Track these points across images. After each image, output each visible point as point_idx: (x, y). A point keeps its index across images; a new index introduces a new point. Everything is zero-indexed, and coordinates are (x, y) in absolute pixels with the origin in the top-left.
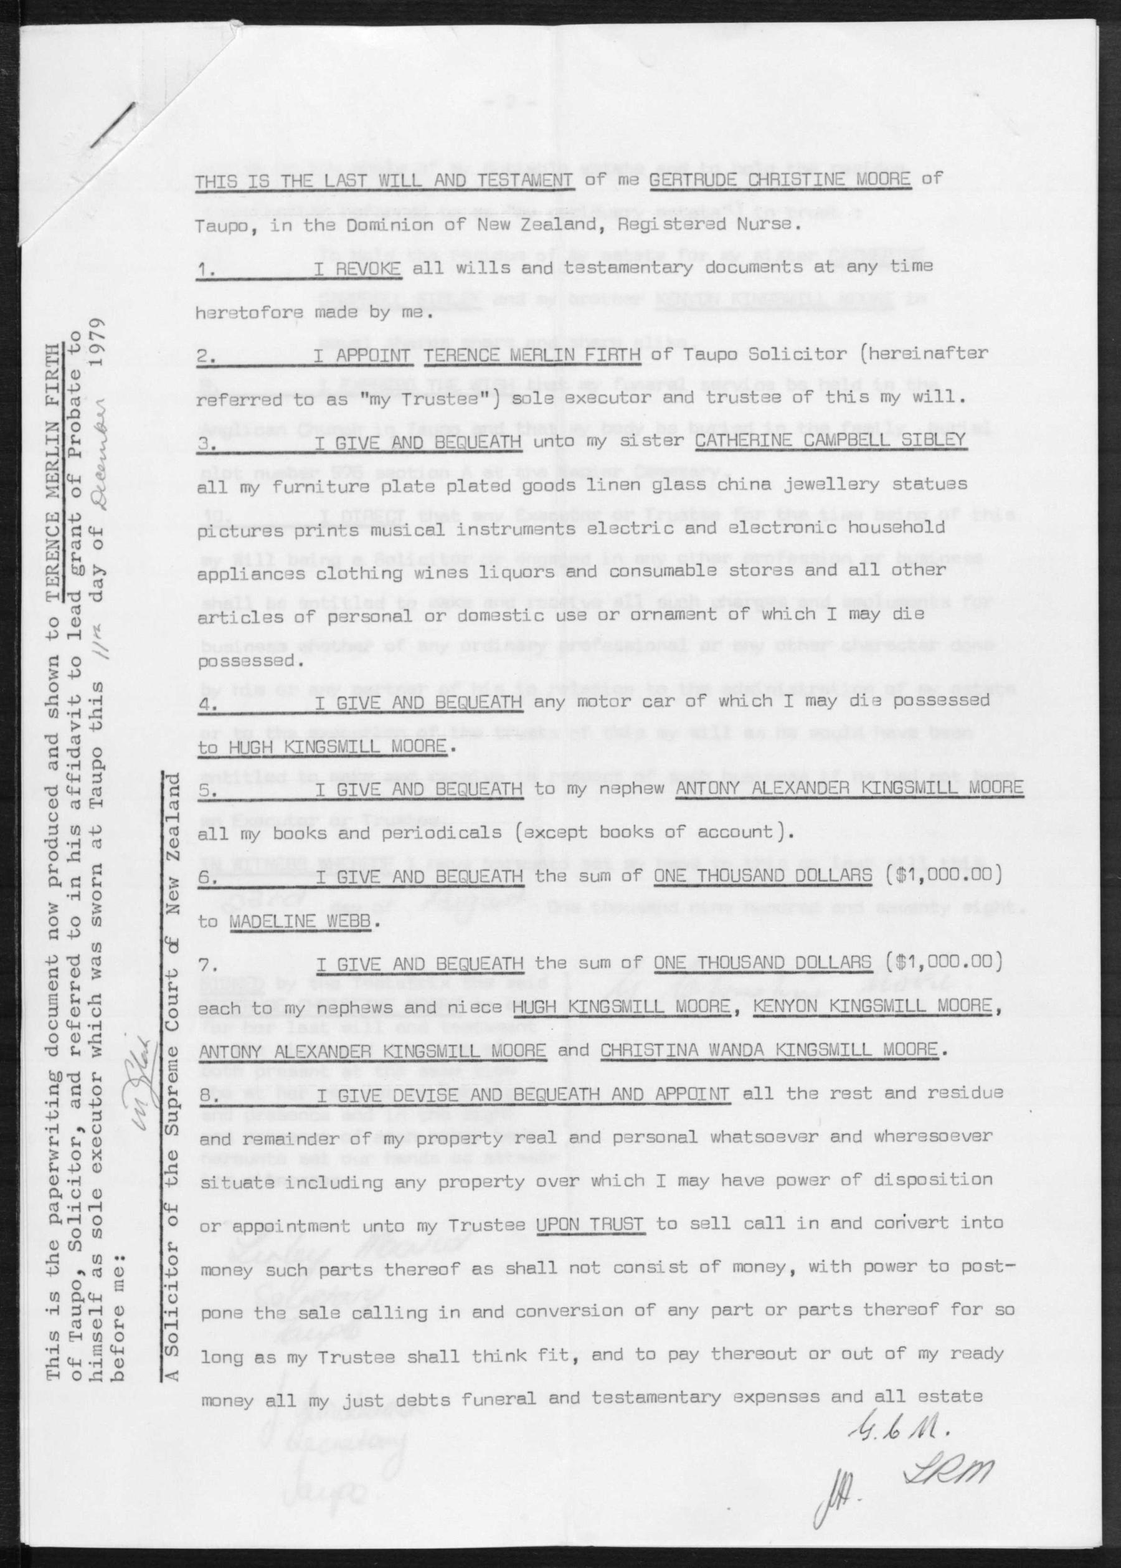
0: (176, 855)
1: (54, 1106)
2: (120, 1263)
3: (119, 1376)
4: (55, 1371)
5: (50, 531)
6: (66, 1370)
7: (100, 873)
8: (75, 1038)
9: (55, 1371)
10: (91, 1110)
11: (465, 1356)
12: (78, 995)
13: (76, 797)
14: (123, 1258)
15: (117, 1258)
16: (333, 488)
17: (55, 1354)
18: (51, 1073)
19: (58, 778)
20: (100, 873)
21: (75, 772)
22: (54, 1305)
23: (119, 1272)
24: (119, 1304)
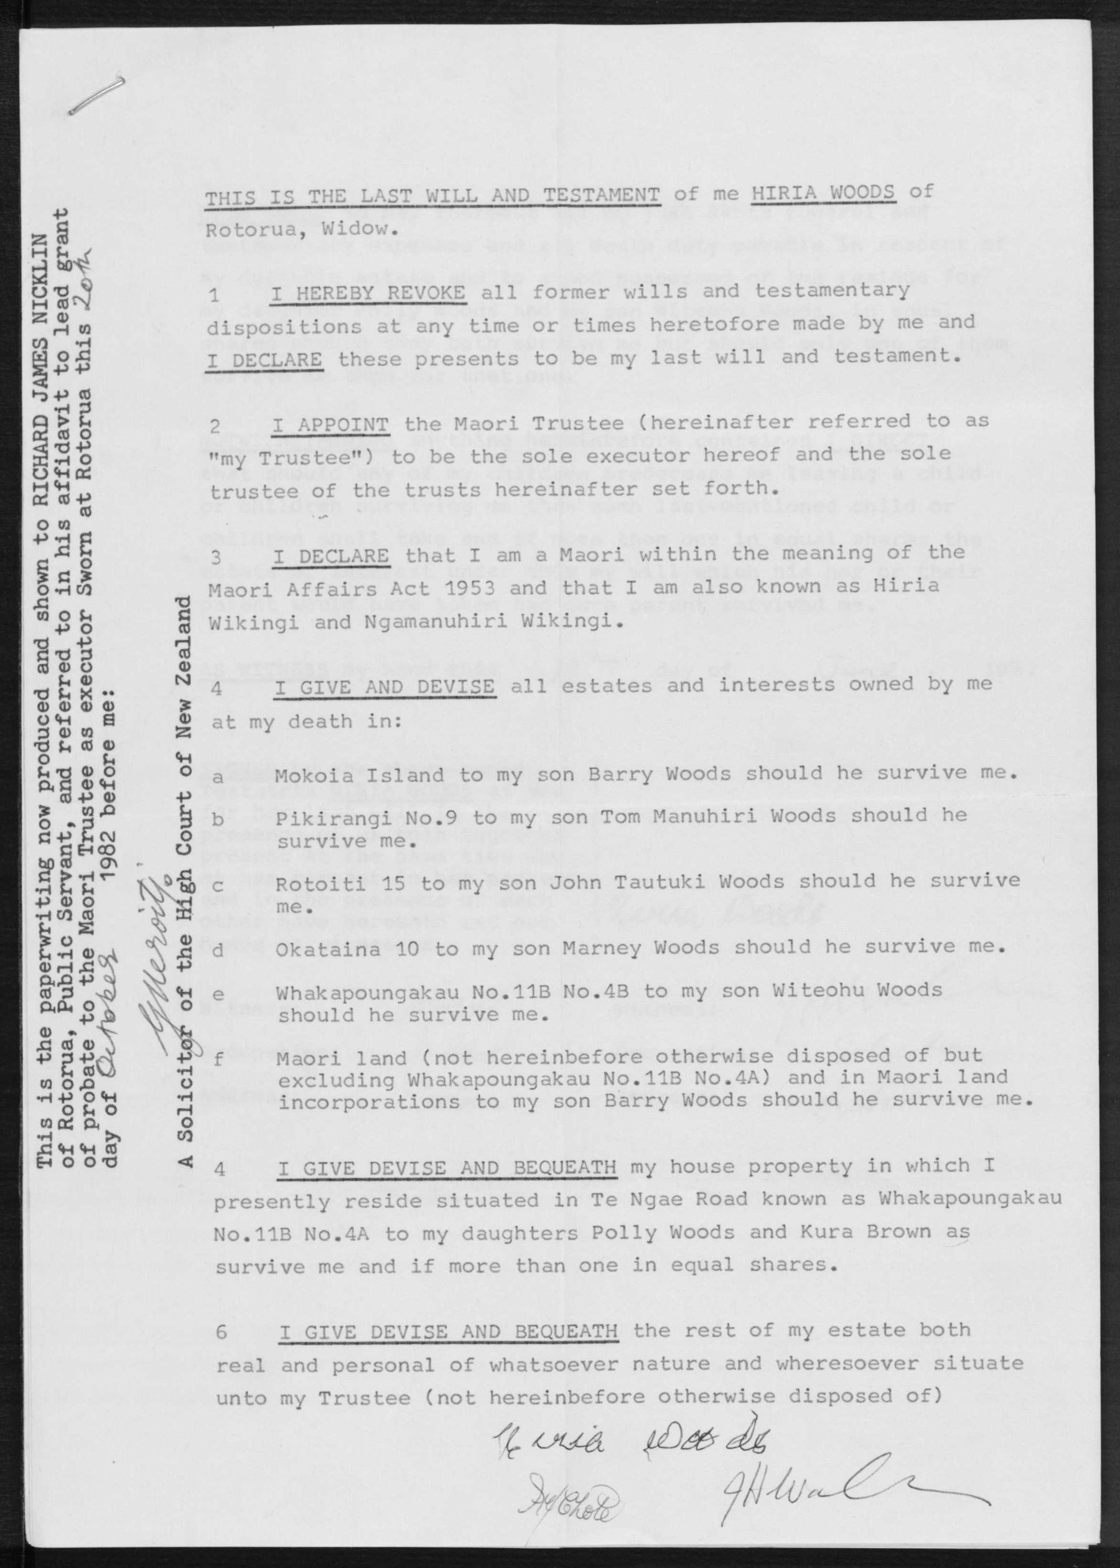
0: (186, 679)
1: (45, 894)
2: (109, 698)
3: (109, 810)
4: (46, 1158)
5: (37, 474)
6: (57, 1157)
7: (90, 541)
8: (64, 733)
9: (46, 1158)
10: (78, 506)
11: (767, 991)
12: (66, 690)
13: (64, 491)
14: (112, 693)
15: (105, 693)
16: (470, 1203)
17: (47, 1141)
18: (41, 861)
19: (50, 681)
20: (90, 541)
21: (63, 467)
22: (45, 1092)
23: (108, 706)
24: (110, 739)
